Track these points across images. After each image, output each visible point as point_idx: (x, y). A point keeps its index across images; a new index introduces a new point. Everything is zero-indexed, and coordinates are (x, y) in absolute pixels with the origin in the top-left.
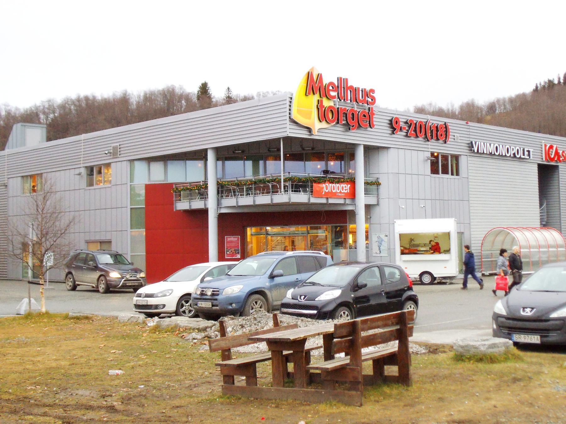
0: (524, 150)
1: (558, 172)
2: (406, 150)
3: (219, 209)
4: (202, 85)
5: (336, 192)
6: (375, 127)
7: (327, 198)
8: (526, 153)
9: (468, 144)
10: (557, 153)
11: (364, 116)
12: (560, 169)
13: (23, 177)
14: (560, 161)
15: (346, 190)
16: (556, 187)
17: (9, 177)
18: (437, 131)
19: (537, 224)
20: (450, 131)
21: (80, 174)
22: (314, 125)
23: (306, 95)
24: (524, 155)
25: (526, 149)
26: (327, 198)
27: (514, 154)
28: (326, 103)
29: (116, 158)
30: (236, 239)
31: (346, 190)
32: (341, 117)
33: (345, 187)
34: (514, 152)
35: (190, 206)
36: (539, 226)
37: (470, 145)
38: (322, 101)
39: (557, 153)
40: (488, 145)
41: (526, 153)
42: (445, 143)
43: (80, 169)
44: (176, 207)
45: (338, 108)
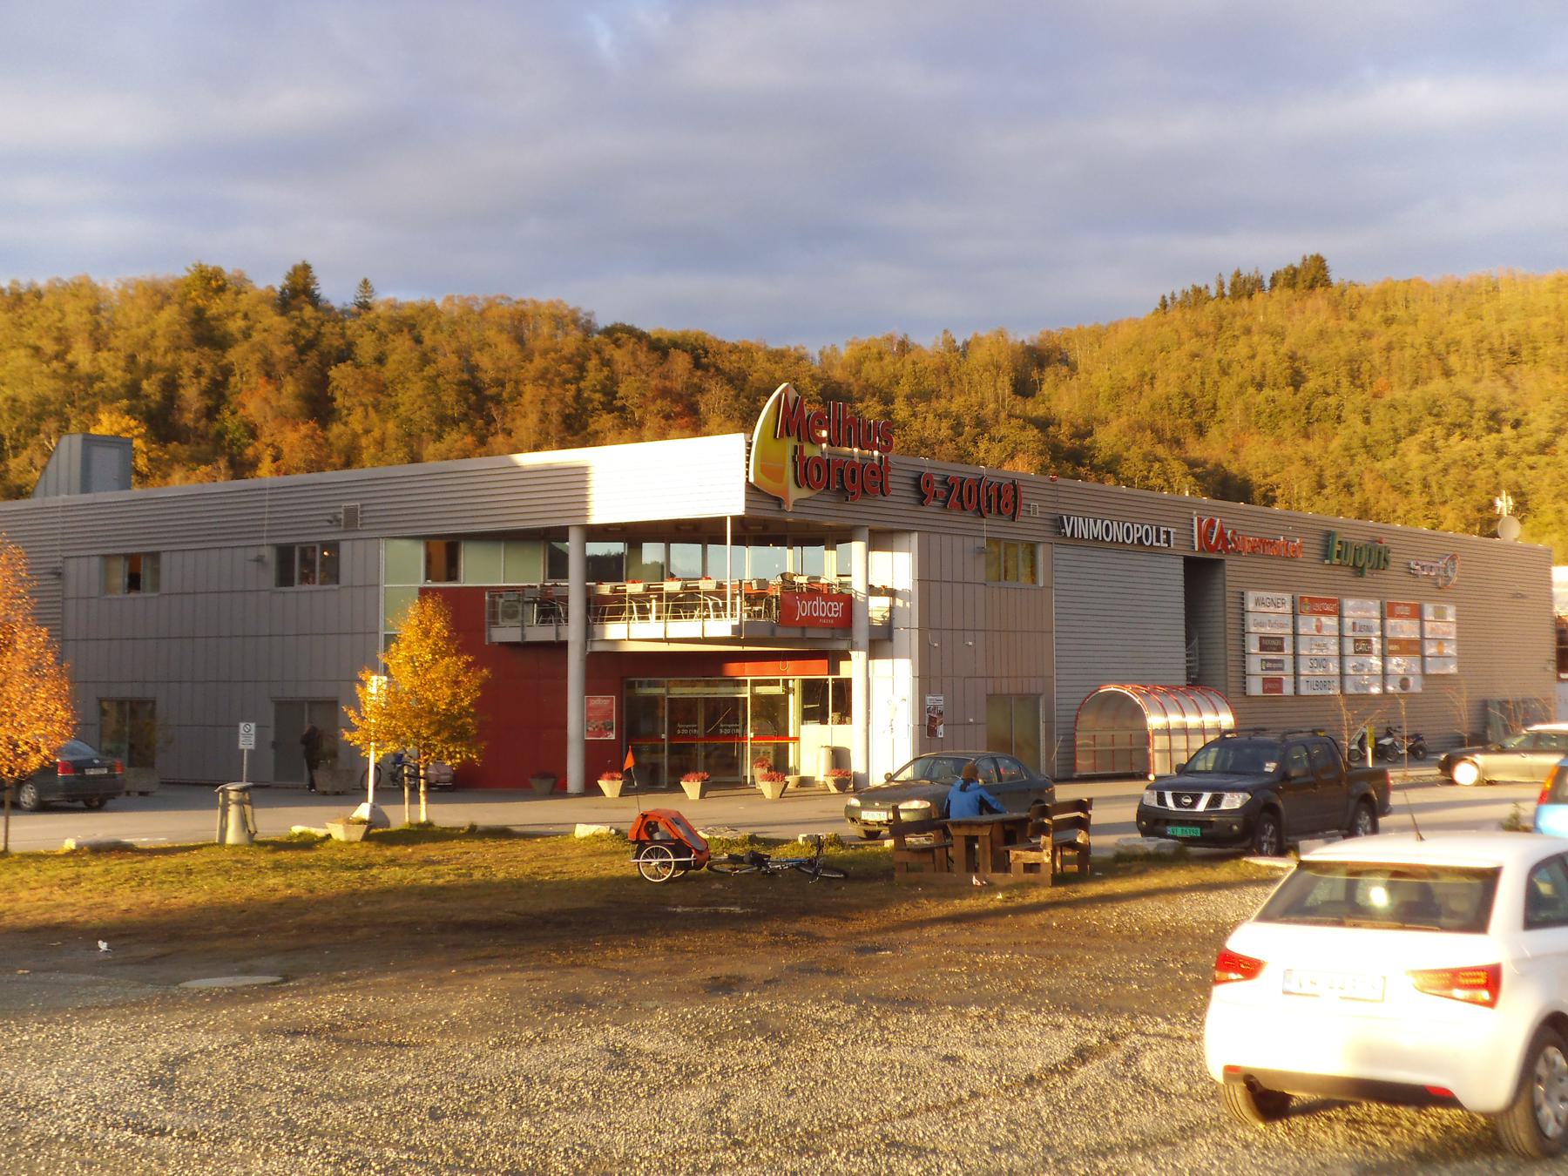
0: (1158, 531)
1: (1224, 569)
2: (954, 537)
3: (589, 643)
4: (295, 269)
5: (820, 617)
6: (893, 492)
7: (803, 628)
8: (1163, 537)
9: (1056, 520)
10: (1222, 534)
11: (873, 473)
12: (1227, 568)
13: (105, 556)
14: (1228, 552)
15: (835, 612)
16: (1220, 614)
17: (65, 554)
18: (999, 497)
19: (1181, 679)
20: (1023, 495)
21: (260, 560)
22: (786, 492)
23: (775, 436)
24: (1158, 541)
25: (1162, 529)
26: (803, 628)
27: (1140, 539)
28: (810, 451)
29: (353, 531)
30: (606, 702)
31: (835, 612)
32: (834, 477)
33: (835, 606)
34: (1139, 535)
35: (523, 636)
36: (1184, 683)
37: (1059, 523)
38: (802, 448)
39: (1222, 534)
40: (1091, 521)
41: (1163, 537)
42: (1013, 520)
43: (261, 548)
44: (490, 636)
45: (828, 460)
